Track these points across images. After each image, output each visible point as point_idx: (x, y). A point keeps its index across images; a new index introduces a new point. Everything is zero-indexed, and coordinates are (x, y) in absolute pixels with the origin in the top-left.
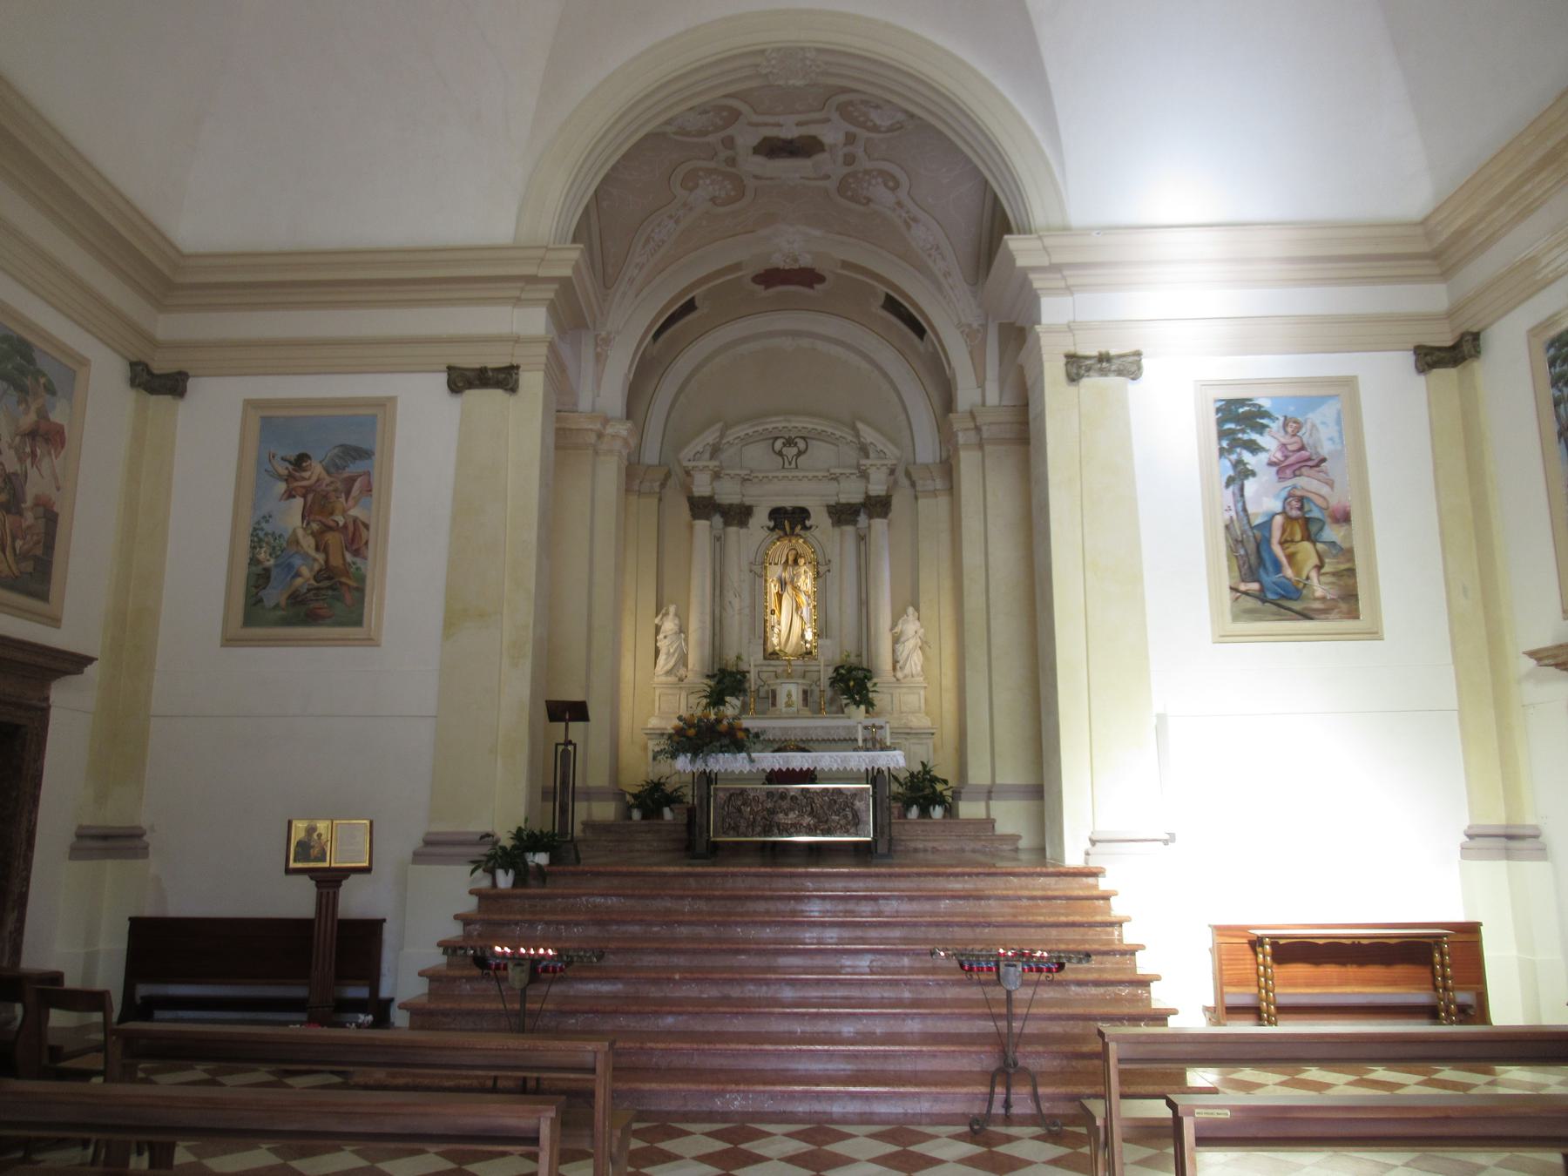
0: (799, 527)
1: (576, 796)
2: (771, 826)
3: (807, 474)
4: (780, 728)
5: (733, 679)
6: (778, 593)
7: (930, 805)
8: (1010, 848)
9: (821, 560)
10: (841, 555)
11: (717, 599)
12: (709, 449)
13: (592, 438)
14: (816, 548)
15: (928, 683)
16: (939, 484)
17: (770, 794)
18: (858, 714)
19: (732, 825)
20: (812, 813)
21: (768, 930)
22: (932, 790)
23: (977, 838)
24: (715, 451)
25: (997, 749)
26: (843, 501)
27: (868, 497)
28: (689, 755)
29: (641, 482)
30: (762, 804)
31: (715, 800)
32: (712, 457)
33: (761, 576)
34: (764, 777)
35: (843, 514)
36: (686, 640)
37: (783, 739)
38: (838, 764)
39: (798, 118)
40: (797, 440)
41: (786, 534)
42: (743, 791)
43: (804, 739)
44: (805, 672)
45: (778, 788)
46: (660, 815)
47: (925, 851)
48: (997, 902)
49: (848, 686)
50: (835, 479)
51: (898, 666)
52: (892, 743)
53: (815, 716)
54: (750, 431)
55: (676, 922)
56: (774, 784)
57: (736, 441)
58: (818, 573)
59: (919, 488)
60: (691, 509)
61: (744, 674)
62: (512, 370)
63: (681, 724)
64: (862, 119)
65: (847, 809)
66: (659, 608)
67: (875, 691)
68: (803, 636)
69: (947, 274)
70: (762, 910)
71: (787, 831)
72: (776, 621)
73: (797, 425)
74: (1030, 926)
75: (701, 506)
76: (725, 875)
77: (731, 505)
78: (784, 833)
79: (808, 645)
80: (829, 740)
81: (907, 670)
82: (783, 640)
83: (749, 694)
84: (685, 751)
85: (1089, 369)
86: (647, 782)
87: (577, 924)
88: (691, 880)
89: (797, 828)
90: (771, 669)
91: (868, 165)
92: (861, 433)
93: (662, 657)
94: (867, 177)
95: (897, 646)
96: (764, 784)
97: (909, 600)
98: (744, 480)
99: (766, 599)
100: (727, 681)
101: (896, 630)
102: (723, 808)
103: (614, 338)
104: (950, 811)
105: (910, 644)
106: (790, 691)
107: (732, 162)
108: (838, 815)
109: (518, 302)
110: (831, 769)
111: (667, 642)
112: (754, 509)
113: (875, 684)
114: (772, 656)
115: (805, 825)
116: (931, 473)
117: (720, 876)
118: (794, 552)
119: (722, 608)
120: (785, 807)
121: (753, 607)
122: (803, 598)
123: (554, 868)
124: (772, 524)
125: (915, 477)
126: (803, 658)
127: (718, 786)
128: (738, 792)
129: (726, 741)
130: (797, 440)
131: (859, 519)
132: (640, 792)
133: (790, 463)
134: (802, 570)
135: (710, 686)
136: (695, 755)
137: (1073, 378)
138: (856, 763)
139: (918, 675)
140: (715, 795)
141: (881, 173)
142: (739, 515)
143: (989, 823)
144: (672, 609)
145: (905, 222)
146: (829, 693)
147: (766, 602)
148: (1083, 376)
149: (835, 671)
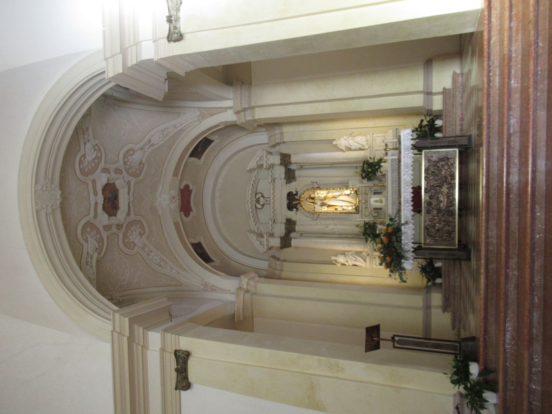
0: (296, 197)
1: (427, 337)
2: (449, 211)
4: (392, 206)
5: (368, 229)
6: (327, 207)
8: (460, 78)
9: (311, 187)
11: (330, 236)
12: (259, 239)
13: (248, 295)
14: (305, 189)
15: (370, 132)
16: (277, 131)
17: (428, 212)
18: (386, 167)
19: (448, 235)
20: (440, 186)
21: (538, 214)
22: (426, 127)
23: (454, 96)
25: (403, 91)
27: (281, 164)
28: (403, 261)
29: (276, 270)
30: (434, 217)
31: (431, 245)
32: (262, 236)
33: (319, 215)
35: (290, 176)
36: (348, 252)
37: (398, 204)
39: (92, 195)
40: (257, 198)
41: (299, 203)
42: (426, 228)
44: (365, 194)
45: (425, 207)
46: (439, 268)
47: (461, 125)
48: (513, 45)
49: (371, 172)
50: (274, 180)
51: (362, 148)
52: (396, 138)
53: (387, 188)
54: (252, 219)
55: (531, 285)
56: (421, 209)
57: (257, 225)
58: (317, 188)
59: (279, 141)
60: (287, 247)
61: (366, 224)
62: (177, 353)
63: (384, 264)
64: (93, 165)
65: (438, 165)
66: (332, 263)
67: (374, 158)
68: (348, 195)
69: (175, 127)
70: (517, 218)
71: (452, 201)
72: (341, 208)
73: (250, 198)
74: (538, 10)
75: (285, 243)
76: (487, 244)
77: (286, 229)
78: (453, 203)
79: (353, 192)
81: (364, 143)
82: (350, 204)
83: (376, 221)
84: (400, 263)
85: (175, 28)
86: (421, 274)
87: (531, 359)
88: (491, 267)
89: (450, 196)
90: (363, 210)
91: (121, 162)
92: (252, 167)
93: (357, 263)
94: (129, 163)
95: (352, 149)
96: (421, 215)
97: (330, 144)
99: (330, 213)
100: (369, 231)
101: (344, 150)
102: (437, 240)
103: (204, 282)
104: (439, 115)
106: (374, 201)
107: (119, 226)
108: (442, 170)
109: (145, 347)
110: (412, 175)
111: (349, 261)
112: (288, 217)
113: (370, 158)
114: (357, 209)
115: (448, 191)
116: (272, 136)
117: (488, 247)
118: (308, 200)
119: (333, 234)
120: (436, 203)
121: (333, 219)
122: (330, 195)
123: (481, 360)
124: (295, 210)
125: (274, 143)
126: (358, 195)
127: (423, 242)
128: (426, 231)
129: (394, 239)
130: (257, 198)
131: (292, 169)
132: (426, 277)
133: (267, 201)
134: (316, 195)
135: (371, 241)
136: (402, 257)
137: (180, 38)
138: (409, 159)
139: (367, 138)
140: (429, 244)
141: (125, 156)
142: (290, 225)
143: (445, 92)
144: (333, 258)
145: (151, 146)
146: (376, 182)
147: (331, 212)
148: (179, 31)
149: (364, 179)
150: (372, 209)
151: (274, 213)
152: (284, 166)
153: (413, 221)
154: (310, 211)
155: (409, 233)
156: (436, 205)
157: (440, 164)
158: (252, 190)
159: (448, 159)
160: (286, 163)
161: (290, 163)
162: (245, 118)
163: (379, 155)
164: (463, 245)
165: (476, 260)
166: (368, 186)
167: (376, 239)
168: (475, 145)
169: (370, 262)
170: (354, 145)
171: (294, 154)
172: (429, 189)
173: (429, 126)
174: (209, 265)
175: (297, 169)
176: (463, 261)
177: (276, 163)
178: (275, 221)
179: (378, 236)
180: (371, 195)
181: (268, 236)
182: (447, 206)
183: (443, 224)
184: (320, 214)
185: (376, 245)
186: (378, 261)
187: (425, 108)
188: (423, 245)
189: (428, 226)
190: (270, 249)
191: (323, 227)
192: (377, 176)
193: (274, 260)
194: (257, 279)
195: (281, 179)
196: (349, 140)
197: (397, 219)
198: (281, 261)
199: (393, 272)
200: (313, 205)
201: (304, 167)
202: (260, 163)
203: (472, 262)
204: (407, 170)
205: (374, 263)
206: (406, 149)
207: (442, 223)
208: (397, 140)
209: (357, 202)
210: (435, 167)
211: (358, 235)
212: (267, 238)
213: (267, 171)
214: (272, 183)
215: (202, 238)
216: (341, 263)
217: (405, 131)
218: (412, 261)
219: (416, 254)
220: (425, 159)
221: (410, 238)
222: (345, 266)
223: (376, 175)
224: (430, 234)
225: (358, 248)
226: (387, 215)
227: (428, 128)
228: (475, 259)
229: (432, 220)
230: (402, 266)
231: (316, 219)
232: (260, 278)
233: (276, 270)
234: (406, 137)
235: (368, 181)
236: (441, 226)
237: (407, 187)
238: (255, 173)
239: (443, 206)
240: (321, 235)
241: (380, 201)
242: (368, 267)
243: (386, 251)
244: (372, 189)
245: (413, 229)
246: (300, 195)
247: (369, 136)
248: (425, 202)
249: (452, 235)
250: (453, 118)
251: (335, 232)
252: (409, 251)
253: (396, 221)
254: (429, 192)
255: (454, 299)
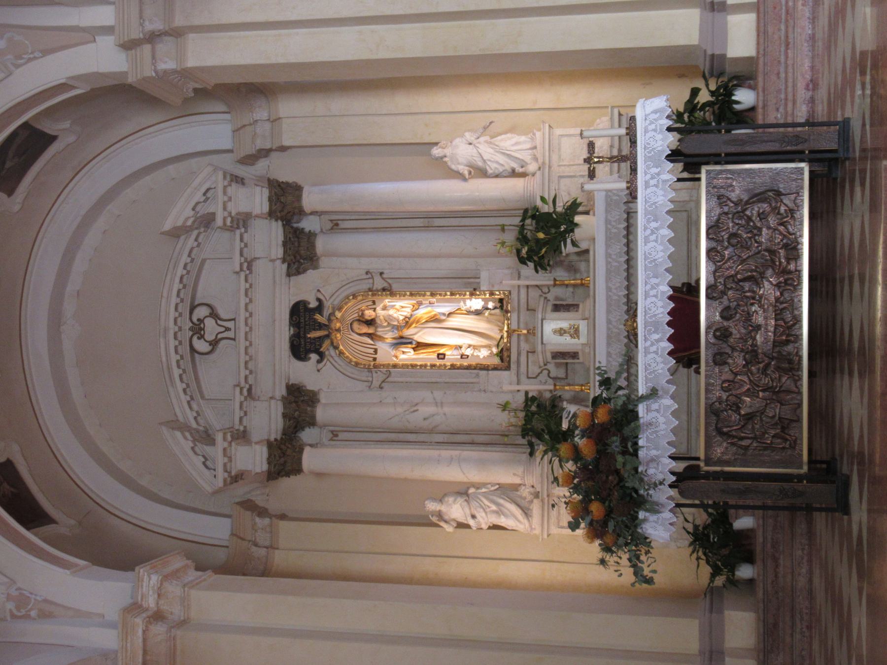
0: (318, 317)
3: (242, 305)
4: (609, 344)
5: (536, 416)
6: (414, 349)
7: (731, 109)
9: (365, 286)
10: (358, 256)
11: (421, 437)
12: (199, 448)
13: (159, 629)
15: (544, 122)
16: (261, 113)
17: (719, 359)
20: (756, 280)
24: (206, 437)
26: (280, 252)
27: (271, 214)
29: (256, 545)
30: (736, 374)
31: (728, 463)
32: (211, 442)
34: (686, 370)
36: (478, 486)
37: (626, 340)
38: (661, 227)
40: (195, 319)
42: (712, 411)
43: (625, 308)
49: (545, 243)
50: (249, 265)
51: (519, 170)
53: (591, 293)
54: (180, 386)
56: (699, 353)
57: (195, 406)
58: (384, 290)
60: (288, 475)
61: (529, 400)
65: (748, 213)
66: (425, 522)
68: (478, 313)
71: (789, 328)
72: (456, 352)
75: (282, 460)
77: (285, 416)
79: (491, 305)
80: (628, 270)
81: (526, 156)
82: (484, 342)
83: (559, 393)
84: (634, 522)
92: (179, 223)
93: (502, 521)
95: (490, 171)
96: (697, 372)
98: (250, 394)
99: (421, 366)
101: (466, 173)
102: (746, 448)
103: (19, 589)
105: (487, 152)
108: (760, 230)
111: (480, 515)
113: (543, 199)
114: (504, 355)
115: (778, 294)
116: (244, 126)
118: (356, 326)
119: (431, 431)
120: (743, 331)
121: (431, 385)
122: (423, 312)
124: (314, 357)
125: (249, 150)
126: (507, 312)
129: (615, 443)
130: (195, 319)
131: (307, 230)
132: (708, 562)
133: (228, 329)
134: (380, 312)
135: (545, 452)
139: (532, 139)
140: (720, 462)
144: (432, 506)
146: (560, 274)
147: (426, 366)
149: (525, 264)
150: (549, 356)
151: (250, 365)
152: (282, 221)
153: (673, 388)
154: (360, 361)
155: (663, 427)
156: (743, 339)
157: (753, 211)
158: (178, 295)
159: (778, 194)
160: (286, 211)
161: (301, 212)
162: (153, 64)
163: (566, 193)
164: (822, 462)
165: (869, 511)
166: (537, 286)
167: (558, 446)
168: (863, 150)
169: (543, 516)
170: (495, 160)
171: (314, 185)
172: (721, 287)
173: (716, 107)
174: (36, 535)
175: (322, 231)
176: (816, 515)
177: (257, 211)
178: (253, 391)
179: (567, 436)
180: (544, 310)
181: (229, 438)
182: (774, 341)
183: (764, 399)
184: (392, 370)
185: (561, 466)
186: (566, 517)
187: (705, 51)
188: (702, 464)
189: (717, 404)
190: (236, 481)
191: (400, 410)
192: (564, 254)
193: (248, 513)
194: (192, 575)
195: (273, 261)
196: (481, 147)
197: (622, 382)
198: (270, 516)
199: (612, 552)
200: (371, 342)
201: (343, 225)
202: (203, 210)
203: (855, 517)
204: (654, 225)
205: (553, 520)
206: (651, 159)
207: (761, 394)
208: (623, 131)
209: (505, 335)
210: (741, 218)
211: (507, 436)
212: (226, 445)
213: (227, 234)
214: (243, 275)
215: (16, 448)
216: (454, 520)
217: (648, 102)
218: (671, 515)
219: (680, 493)
220: (708, 192)
221: (664, 443)
222: (468, 530)
223: (561, 253)
224: (725, 430)
225: (507, 476)
226: (592, 369)
227: (714, 113)
228: (865, 506)
229: (729, 385)
230: (639, 531)
231: (381, 388)
232: (200, 573)
233: (256, 545)
234: (651, 123)
235: (537, 271)
236: (758, 404)
237: (654, 281)
238: (191, 242)
239: (763, 343)
240: (393, 436)
241: (572, 331)
242: (537, 531)
243: (590, 483)
244: (549, 296)
245: (675, 414)
246: (330, 311)
247: (538, 134)
248: (708, 328)
249: (792, 432)
250: (786, 81)
251: (436, 427)
252: (661, 483)
253: (620, 388)
254: (722, 298)
255: (793, 627)
